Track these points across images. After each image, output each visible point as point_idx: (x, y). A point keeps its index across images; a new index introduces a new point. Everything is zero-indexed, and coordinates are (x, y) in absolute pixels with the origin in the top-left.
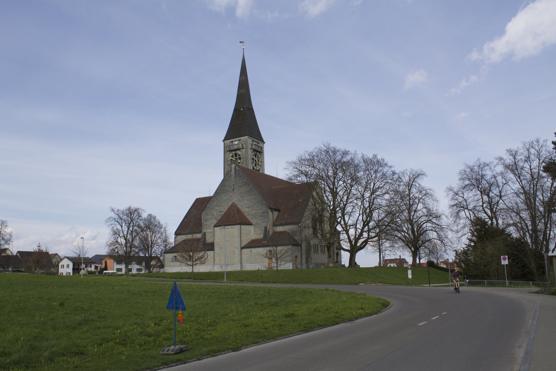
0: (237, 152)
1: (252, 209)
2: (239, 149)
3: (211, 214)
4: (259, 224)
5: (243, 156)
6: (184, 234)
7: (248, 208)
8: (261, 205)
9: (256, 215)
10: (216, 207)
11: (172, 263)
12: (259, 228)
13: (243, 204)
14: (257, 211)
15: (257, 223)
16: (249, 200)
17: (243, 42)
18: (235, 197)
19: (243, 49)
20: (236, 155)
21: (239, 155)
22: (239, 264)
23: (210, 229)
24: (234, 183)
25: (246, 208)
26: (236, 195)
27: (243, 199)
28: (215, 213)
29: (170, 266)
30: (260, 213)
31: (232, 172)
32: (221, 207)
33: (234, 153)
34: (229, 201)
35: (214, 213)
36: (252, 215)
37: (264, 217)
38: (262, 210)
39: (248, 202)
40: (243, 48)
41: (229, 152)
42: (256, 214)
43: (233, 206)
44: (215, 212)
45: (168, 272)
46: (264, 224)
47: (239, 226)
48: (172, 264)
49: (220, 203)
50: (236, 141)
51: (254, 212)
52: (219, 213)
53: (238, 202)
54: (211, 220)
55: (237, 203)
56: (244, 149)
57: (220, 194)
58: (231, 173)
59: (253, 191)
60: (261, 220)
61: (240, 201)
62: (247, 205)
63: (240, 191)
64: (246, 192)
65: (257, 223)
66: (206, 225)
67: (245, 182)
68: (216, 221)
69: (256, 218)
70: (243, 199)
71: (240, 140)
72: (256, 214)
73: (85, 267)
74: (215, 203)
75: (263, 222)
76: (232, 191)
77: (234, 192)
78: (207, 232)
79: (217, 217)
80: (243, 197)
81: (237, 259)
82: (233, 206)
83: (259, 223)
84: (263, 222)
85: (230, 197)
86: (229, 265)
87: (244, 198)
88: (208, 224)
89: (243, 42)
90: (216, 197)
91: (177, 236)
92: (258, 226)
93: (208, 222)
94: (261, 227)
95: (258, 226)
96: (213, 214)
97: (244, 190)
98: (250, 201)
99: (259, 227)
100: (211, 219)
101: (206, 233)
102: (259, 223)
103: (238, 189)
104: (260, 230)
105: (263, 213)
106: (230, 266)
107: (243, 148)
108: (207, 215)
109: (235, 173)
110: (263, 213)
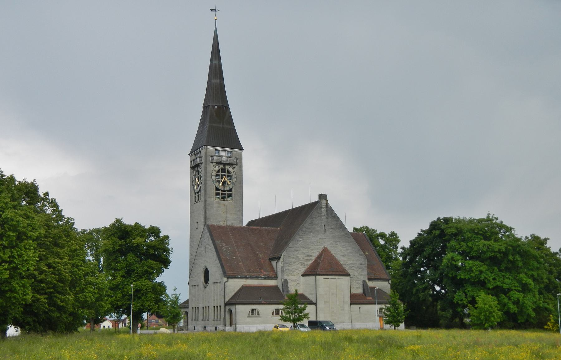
0: (227, 167)
1: (349, 259)
2: (231, 165)
3: (295, 257)
4: (356, 276)
5: (236, 175)
6: (242, 278)
7: (344, 256)
8: (358, 255)
9: (353, 267)
10: (302, 249)
11: (248, 318)
12: (357, 282)
13: (337, 250)
14: (354, 261)
15: (354, 275)
16: (344, 248)
17: (215, 10)
18: (326, 240)
19: (216, 20)
20: (223, 170)
21: (229, 172)
22: (349, 323)
23: (294, 275)
24: (325, 223)
25: (341, 255)
26: (328, 238)
27: (337, 245)
28: (300, 257)
29: (246, 323)
30: (357, 264)
31: (322, 209)
32: (309, 250)
33: (221, 167)
34: (319, 244)
35: (298, 255)
36: (348, 265)
37: (362, 270)
38: (360, 262)
39: (343, 249)
40: (216, 18)
41: (214, 165)
42: (353, 265)
43: (325, 251)
44: (300, 255)
45: (243, 330)
46: (362, 277)
47: (314, 277)
48: (249, 320)
49: (307, 244)
50: (225, 151)
51: (350, 262)
52: (306, 256)
53: (331, 247)
54: (295, 264)
55: (329, 248)
56: (237, 166)
57: (307, 233)
58: (321, 210)
59: (349, 238)
60: (358, 272)
61: (334, 247)
62: (342, 252)
63: (333, 235)
64: (341, 237)
65: (354, 275)
66: (288, 270)
67: (340, 225)
68: (304, 268)
69: (353, 270)
70: (337, 245)
71: (231, 152)
72: (353, 265)
73: (310, 319)
74: (300, 243)
75: (361, 275)
76: (323, 233)
77: (326, 234)
78: (289, 280)
79: (303, 262)
80: (337, 242)
81: (347, 317)
82: (325, 251)
83: (356, 275)
84: (361, 275)
85: (320, 239)
86: (337, 323)
87: (338, 243)
88: (290, 268)
89: (215, 10)
90: (301, 236)
91: (230, 280)
92: (356, 279)
93: (290, 266)
94: (359, 281)
95: (356, 279)
96: (298, 257)
97: (338, 234)
98: (345, 249)
99: (356, 280)
100: (295, 263)
101: (288, 281)
102: (356, 275)
103: (331, 231)
104: (358, 283)
105: (361, 264)
106: (339, 324)
107: (237, 165)
108: (289, 257)
109: (327, 211)
110: (361, 264)
